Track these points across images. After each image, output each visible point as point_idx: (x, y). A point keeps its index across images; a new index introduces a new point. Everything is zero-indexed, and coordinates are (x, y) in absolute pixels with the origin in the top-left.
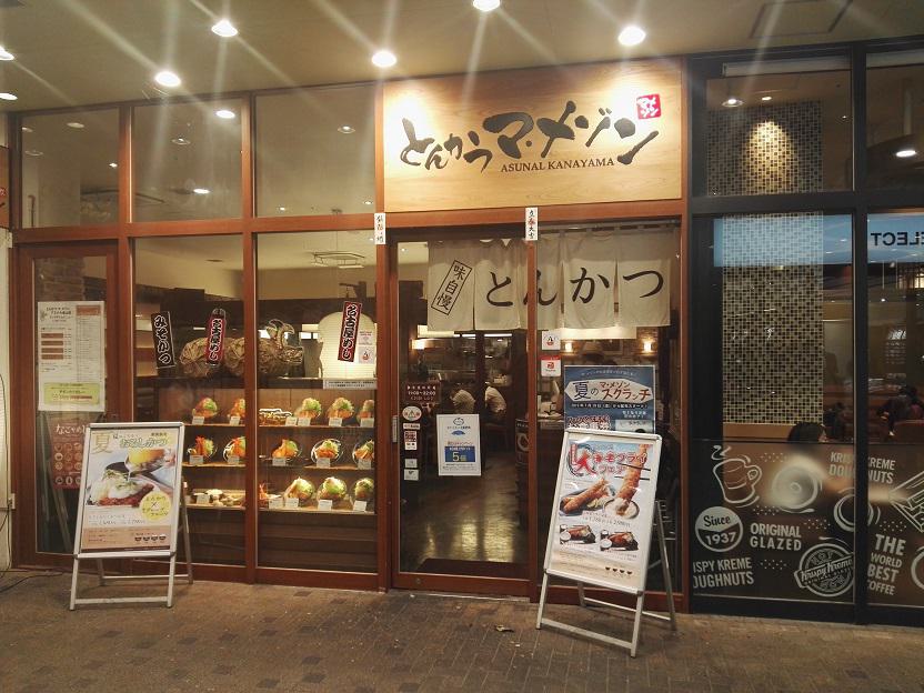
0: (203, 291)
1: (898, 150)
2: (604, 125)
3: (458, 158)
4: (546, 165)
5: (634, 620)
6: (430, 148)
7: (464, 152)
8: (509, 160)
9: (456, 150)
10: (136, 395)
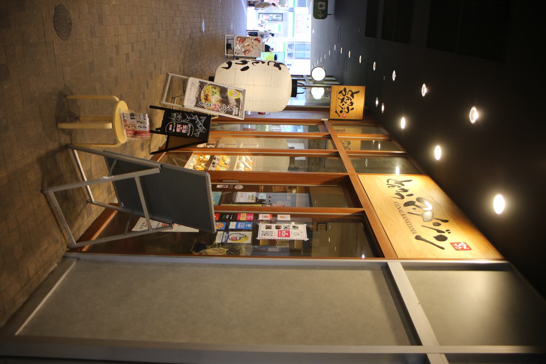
0: (281, 7)
1: (350, 52)
2: (342, 108)
3: (348, 105)
4: (337, 98)
5: (171, 103)
6: (351, 98)
7: (349, 106)
8: (338, 92)
9: (350, 104)
10: (261, 185)
